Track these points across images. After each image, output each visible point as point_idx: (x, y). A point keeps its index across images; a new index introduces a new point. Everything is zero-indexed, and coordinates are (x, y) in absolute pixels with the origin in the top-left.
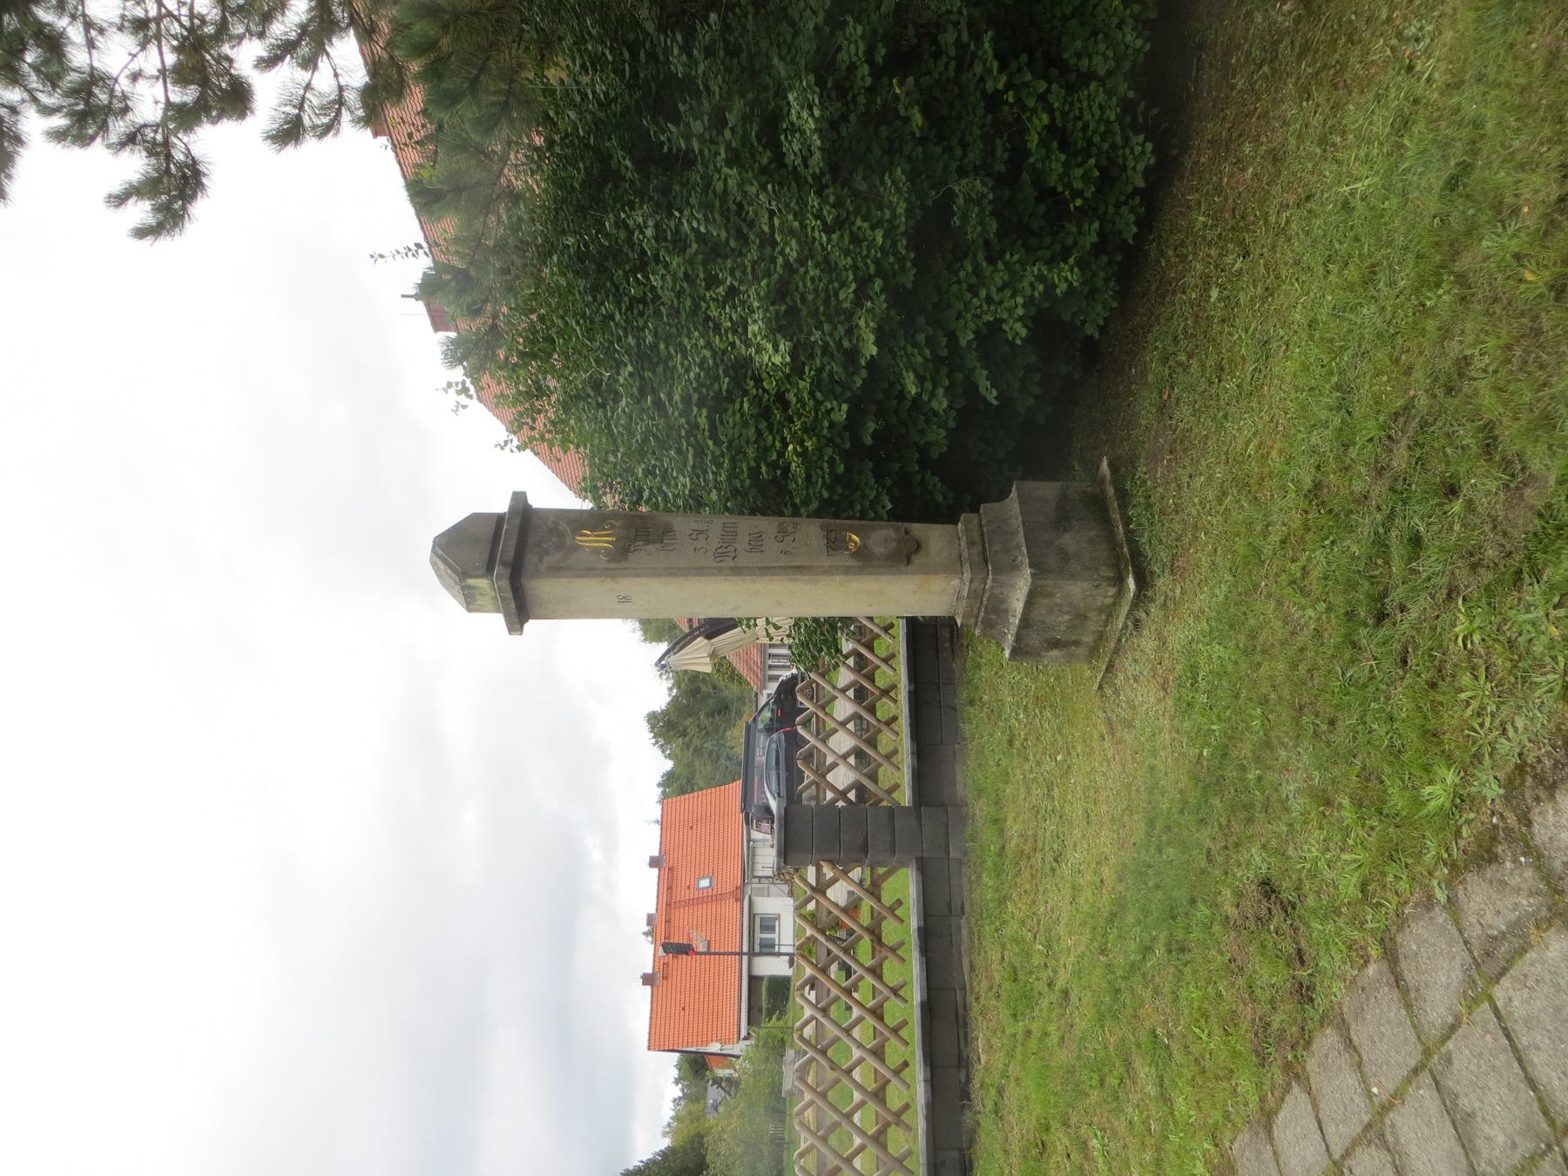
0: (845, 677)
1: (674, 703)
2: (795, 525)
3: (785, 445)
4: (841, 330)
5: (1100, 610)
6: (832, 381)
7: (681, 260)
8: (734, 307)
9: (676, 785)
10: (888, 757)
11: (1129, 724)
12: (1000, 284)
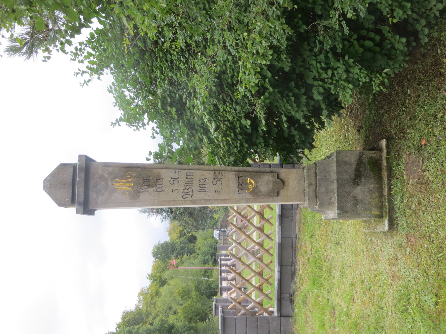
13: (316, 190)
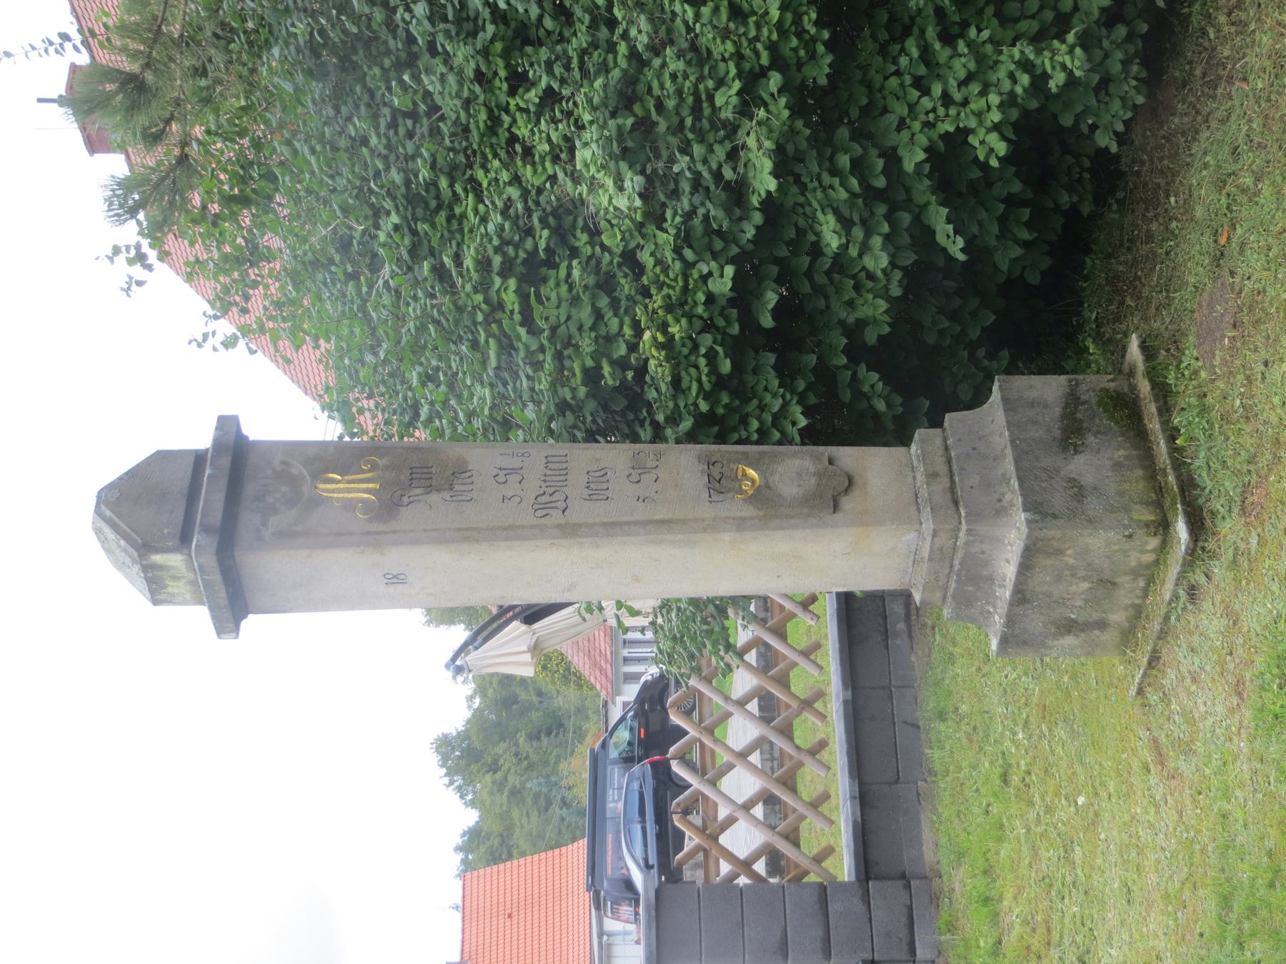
0: (743, 682)
1: (477, 719)
2: (659, 456)
3: (639, 332)
4: (720, 152)
5: (1135, 574)
6: (709, 231)
7: (469, 50)
8: (554, 121)
9: (486, 849)
10: (815, 805)
11: (1186, 749)
12: (962, 74)
13: (952, 489)
